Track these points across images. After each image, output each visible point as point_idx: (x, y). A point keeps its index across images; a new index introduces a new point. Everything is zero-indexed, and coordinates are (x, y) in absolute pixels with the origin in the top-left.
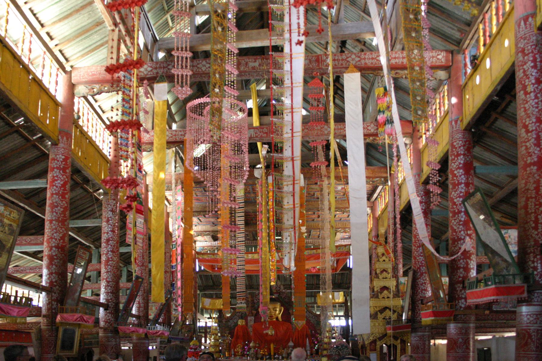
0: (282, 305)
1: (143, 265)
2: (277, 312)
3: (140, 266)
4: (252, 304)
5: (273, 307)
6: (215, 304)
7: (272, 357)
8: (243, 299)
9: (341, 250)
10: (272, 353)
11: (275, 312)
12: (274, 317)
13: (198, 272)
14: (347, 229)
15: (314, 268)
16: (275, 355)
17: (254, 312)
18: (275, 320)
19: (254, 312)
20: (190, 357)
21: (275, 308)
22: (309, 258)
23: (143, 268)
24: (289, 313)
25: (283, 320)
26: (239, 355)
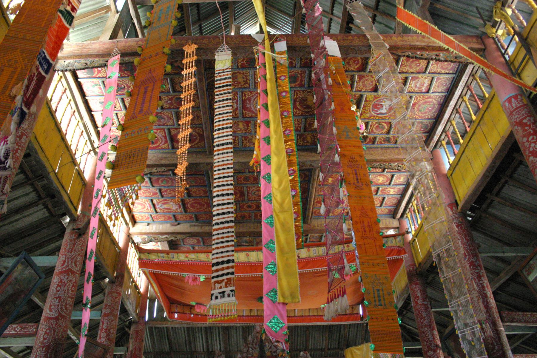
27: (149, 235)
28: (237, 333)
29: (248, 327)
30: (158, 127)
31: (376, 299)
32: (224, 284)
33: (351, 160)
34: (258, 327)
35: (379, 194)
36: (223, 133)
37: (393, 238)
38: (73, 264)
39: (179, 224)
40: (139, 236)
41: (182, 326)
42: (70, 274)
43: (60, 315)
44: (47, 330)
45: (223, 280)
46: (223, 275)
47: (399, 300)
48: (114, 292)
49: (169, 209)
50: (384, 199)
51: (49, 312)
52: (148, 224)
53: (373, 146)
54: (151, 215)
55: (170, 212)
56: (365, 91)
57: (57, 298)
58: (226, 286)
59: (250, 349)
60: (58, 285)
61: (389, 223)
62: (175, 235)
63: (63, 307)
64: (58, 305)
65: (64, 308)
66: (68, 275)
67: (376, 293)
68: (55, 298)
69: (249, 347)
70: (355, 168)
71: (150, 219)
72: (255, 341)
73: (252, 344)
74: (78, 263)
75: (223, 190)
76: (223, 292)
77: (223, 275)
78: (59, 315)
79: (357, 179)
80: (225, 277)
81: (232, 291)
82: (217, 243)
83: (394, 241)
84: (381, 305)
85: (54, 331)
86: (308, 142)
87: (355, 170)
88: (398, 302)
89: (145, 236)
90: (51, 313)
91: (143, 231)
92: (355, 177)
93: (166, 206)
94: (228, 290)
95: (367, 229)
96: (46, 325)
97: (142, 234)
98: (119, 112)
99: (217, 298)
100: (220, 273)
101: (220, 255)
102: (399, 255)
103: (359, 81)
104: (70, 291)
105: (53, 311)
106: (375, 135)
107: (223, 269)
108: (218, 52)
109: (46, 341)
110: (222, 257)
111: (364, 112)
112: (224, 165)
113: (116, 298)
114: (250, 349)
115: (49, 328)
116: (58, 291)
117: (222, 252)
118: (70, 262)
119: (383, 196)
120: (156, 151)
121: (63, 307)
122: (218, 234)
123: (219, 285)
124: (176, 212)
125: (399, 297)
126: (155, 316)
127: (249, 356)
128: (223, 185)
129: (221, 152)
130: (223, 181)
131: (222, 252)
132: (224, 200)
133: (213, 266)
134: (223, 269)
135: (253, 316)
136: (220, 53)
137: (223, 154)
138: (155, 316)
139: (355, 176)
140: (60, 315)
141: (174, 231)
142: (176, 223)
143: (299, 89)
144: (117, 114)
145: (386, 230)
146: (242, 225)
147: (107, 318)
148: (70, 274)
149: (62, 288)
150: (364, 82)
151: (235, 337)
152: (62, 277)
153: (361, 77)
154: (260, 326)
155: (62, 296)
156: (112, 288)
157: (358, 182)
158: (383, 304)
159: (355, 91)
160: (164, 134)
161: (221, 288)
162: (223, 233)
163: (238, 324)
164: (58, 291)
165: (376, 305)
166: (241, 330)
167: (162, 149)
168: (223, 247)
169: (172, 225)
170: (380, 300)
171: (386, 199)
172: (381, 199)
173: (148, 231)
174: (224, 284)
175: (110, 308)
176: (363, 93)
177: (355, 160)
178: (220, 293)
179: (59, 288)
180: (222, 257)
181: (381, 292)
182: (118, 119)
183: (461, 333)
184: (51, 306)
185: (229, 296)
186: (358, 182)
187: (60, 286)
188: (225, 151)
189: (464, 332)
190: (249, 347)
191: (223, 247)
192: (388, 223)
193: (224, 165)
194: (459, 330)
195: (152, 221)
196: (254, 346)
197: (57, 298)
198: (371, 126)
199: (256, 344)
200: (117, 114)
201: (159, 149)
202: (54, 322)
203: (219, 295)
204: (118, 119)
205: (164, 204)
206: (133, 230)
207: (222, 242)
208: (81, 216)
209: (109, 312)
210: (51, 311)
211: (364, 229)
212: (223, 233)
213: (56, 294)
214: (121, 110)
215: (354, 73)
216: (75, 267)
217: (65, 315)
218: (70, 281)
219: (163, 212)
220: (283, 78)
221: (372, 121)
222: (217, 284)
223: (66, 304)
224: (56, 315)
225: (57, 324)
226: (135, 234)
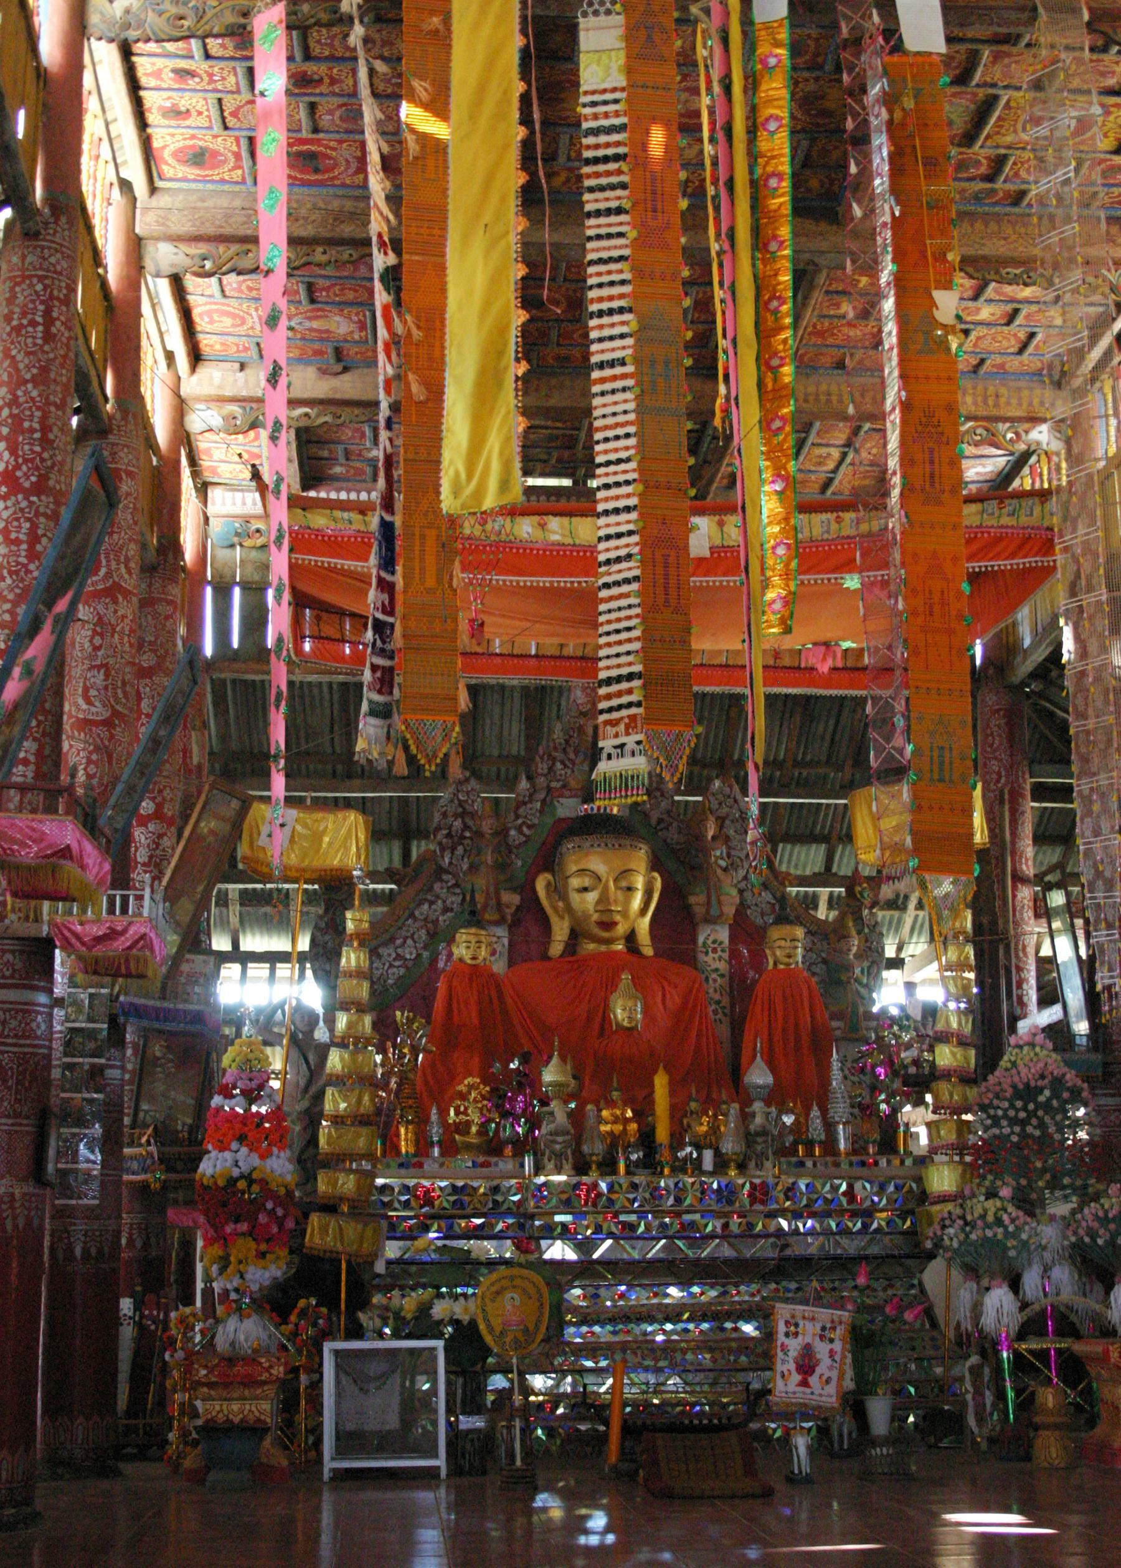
0: (656, 864)
1: (39, 488)
2: (637, 902)
3: (27, 494)
4: (496, 850)
5: (619, 864)
6: (317, 837)
7: (664, 1155)
8: (632, 724)
9: (1024, 520)
10: (662, 1134)
11: (628, 901)
12: (621, 929)
13: (209, 665)
14: (1002, 427)
15: (827, 645)
16: (677, 1143)
17: (512, 899)
18: (619, 947)
19: (512, 899)
20: (223, 1148)
21: (626, 872)
22: (128, 968)
23: (44, 502)
24: (687, 908)
25: (657, 954)
26: (468, 1147)
27: (248, 406)
28: (503, 704)
29: (543, 687)
30: (345, 136)
31: (936, 767)
32: (622, 727)
33: (924, 420)
34: (579, 693)
35: (1017, 322)
36: (613, 325)
37: (1037, 500)
38: (123, 570)
39: (346, 369)
40: (212, 405)
41: (325, 678)
42: (120, 599)
43: (115, 713)
44: (91, 753)
45: (622, 718)
46: (620, 707)
47: (1040, 642)
48: (161, 600)
49: (327, 331)
50: (1032, 335)
51: (84, 706)
52: (242, 367)
53: (1016, 210)
54: (258, 344)
55: (327, 340)
56: (1006, 87)
57: (99, 667)
58: (628, 734)
59: (559, 766)
60: (95, 632)
61: (1042, 403)
62: (332, 409)
63: (119, 691)
64: (106, 688)
65: (121, 695)
66: (115, 601)
67: (936, 753)
68: (92, 667)
69: (554, 760)
70: (931, 445)
71: (254, 352)
72: (575, 740)
73: (564, 751)
74: (132, 565)
75: (617, 498)
76: (622, 746)
77: (620, 707)
78: (113, 715)
79: (932, 476)
80: (624, 713)
81: (639, 743)
82: (608, 634)
83: (1037, 511)
84: (941, 780)
85: (110, 757)
86: (809, 190)
87: (931, 451)
88: (1035, 645)
89: (234, 408)
90: (93, 709)
91: (228, 393)
92: (928, 471)
93: (315, 324)
94: (630, 740)
95: (937, 609)
96: (85, 742)
97: (222, 400)
98: (230, 96)
99: (609, 757)
100: (615, 702)
101: (615, 661)
102: (1044, 555)
103: (994, 63)
104: (127, 648)
105: (97, 704)
106: (1024, 187)
107: (619, 694)
108: (585, 14)
109: (95, 781)
110: (619, 666)
111: (998, 133)
112: (617, 425)
113: (167, 618)
114: (559, 766)
115: (97, 749)
116: (97, 649)
117: (618, 655)
118: (113, 565)
119: (1029, 330)
120: (324, 191)
121: (119, 691)
122: (610, 611)
123: (614, 730)
124: (346, 341)
125: (1040, 630)
126: (236, 645)
127: (554, 784)
128: (618, 484)
129: (608, 386)
130: (615, 473)
131: (618, 655)
132: (618, 524)
133: (600, 686)
134: (619, 694)
135: (569, 658)
136: (591, 19)
137: (613, 392)
138: (236, 645)
139: (927, 466)
140: (115, 713)
141: (331, 395)
142: (339, 368)
143: (806, 74)
144: (220, 100)
145: (1026, 426)
146: (554, 381)
147: (147, 681)
148: (120, 599)
149: (108, 639)
150: (1008, 66)
151: (496, 717)
152: (101, 609)
153: (996, 57)
154: (584, 689)
155: (111, 661)
156: (150, 586)
157: (932, 484)
158: (947, 778)
159: (978, 85)
160: (359, 154)
161: (616, 736)
162: (620, 609)
163: (513, 681)
164: (97, 649)
165: (932, 779)
166: (517, 695)
167: (344, 185)
168: (620, 643)
169: (323, 372)
170: (941, 770)
171: (1039, 337)
172: (1022, 335)
173: (244, 393)
174: (622, 727)
175: (154, 651)
176: (1001, 92)
177: (935, 420)
178: (615, 747)
179: (97, 641)
180: (619, 666)
181: (947, 754)
182: (222, 111)
183: (1085, 844)
184: (86, 689)
185: (633, 754)
186: (932, 484)
187: (102, 635)
188: (619, 384)
189: (1090, 843)
190: (554, 760)
191: (620, 643)
192: (1036, 402)
193: (617, 425)
194: (1083, 837)
195: (256, 356)
196: (572, 756)
197: (99, 667)
198: (1015, 164)
199: (576, 752)
200: (220, 100)
201: (334, 186)
202: (102, 731)
203: (614, 752)
204: (222, 111)
205: (310, 319)
206: (193, 385)
207: (618, 631)
208: (118, 416)
209: (152, 663)
210: (88, 701)
211: (931, 607)
212: (620, 609)
213: (92, 657)
214: (238, 92)
215: (980, 47)
216: (126, 576)
217: (126, 712)
218: (124, 617)
219: (303, 339)
220: (772, 126)
221: (1018, 152)
222: (608, 728)
223: (124, 683)
224: (106, 714)
225: (112, 737)
226: (199, 399)
